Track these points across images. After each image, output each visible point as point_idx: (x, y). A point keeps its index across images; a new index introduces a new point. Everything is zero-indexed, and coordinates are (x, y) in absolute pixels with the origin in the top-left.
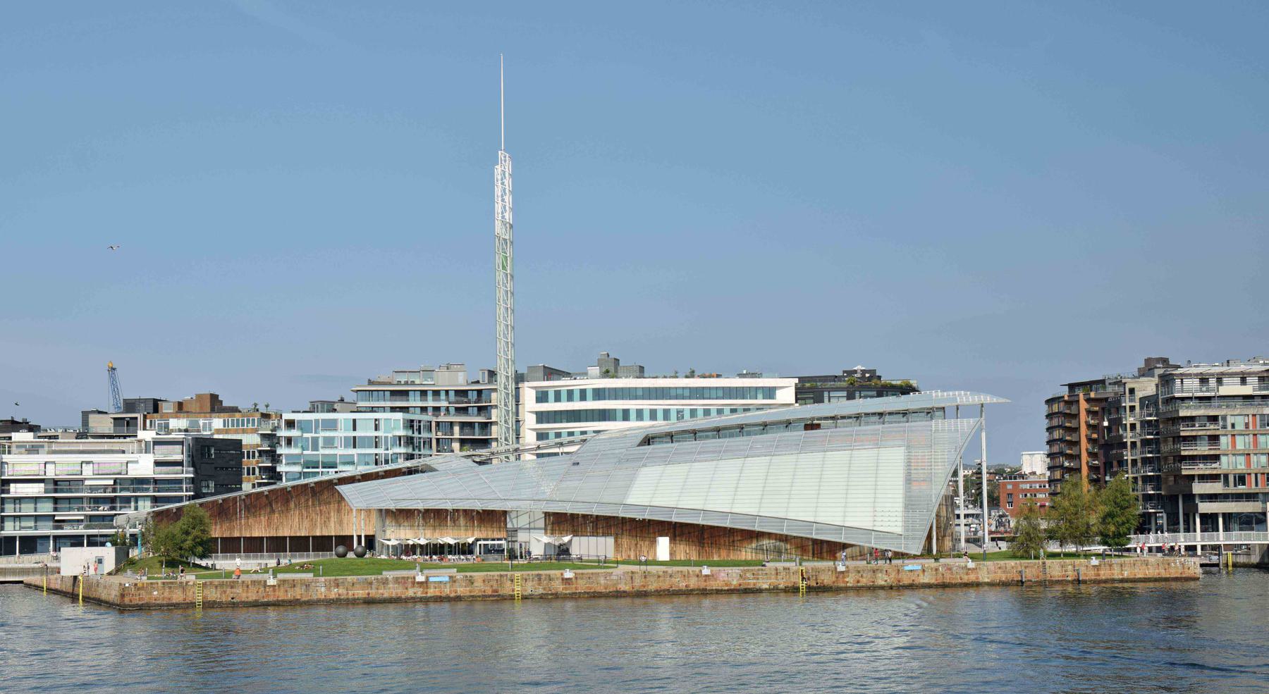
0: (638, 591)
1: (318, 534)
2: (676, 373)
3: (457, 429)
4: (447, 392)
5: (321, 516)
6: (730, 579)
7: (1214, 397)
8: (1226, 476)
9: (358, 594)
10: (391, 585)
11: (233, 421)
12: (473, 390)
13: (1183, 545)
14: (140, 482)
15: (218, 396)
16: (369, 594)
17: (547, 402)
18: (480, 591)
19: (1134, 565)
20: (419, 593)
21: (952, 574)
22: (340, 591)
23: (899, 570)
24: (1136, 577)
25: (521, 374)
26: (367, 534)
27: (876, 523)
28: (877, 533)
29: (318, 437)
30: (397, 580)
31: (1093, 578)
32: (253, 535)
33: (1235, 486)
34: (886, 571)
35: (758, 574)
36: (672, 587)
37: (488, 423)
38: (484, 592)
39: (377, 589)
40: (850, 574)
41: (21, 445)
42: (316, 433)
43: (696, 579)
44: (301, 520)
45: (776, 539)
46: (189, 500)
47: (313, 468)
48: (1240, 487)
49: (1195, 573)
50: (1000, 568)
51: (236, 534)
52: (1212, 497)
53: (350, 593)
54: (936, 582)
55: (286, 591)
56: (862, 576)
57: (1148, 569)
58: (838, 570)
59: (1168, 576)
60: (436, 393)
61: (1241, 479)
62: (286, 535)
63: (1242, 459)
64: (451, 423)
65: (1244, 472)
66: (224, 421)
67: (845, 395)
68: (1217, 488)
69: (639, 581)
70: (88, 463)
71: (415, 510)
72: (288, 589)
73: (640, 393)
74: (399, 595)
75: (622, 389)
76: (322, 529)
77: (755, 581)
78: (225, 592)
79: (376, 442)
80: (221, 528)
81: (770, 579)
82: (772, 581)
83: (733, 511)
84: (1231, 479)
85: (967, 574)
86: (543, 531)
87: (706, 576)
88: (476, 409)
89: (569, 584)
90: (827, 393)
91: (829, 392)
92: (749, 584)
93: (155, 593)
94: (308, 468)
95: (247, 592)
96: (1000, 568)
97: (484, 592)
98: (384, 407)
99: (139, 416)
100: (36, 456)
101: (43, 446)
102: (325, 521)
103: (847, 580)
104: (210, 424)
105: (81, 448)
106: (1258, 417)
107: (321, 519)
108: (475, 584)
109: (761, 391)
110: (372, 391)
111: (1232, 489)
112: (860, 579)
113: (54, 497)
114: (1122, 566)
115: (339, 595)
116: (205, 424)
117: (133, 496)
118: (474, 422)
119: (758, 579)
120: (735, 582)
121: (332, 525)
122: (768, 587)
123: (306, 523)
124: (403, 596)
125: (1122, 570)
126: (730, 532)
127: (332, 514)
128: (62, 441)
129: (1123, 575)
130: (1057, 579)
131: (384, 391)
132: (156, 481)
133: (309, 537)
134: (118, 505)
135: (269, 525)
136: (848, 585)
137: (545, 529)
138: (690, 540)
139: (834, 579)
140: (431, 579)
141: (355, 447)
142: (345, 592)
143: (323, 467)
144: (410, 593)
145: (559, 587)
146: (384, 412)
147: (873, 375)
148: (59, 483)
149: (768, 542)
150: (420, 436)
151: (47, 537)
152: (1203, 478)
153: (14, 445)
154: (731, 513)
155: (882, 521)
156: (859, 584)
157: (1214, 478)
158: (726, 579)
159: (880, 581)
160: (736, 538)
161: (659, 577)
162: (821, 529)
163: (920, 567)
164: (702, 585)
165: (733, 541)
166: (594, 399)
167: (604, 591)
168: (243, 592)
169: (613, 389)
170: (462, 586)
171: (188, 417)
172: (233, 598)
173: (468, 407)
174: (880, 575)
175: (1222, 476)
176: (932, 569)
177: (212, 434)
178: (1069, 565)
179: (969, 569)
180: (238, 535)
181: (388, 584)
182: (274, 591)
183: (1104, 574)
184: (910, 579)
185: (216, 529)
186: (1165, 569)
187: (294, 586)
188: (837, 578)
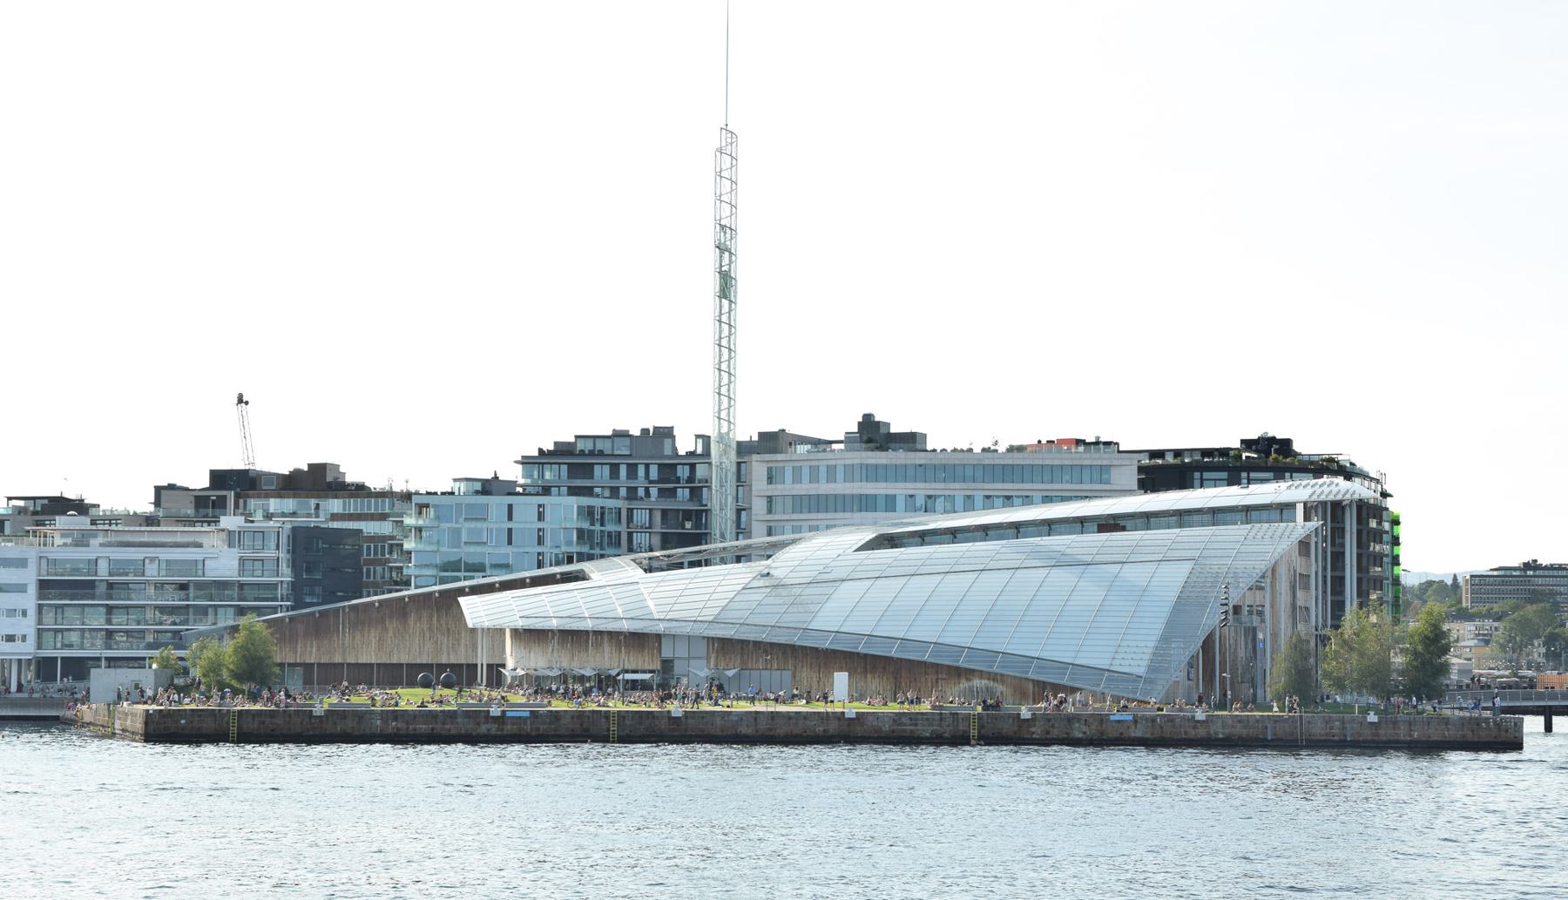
0: (763, 735)
5: (448, 636)
6: (880, 724)
9: (421, 729)
12: (684, 464)
14: (222, 585)
15: (339, 466)
16: (433, 729)
19: (1429, 723)
20: (494, 729)
21: (1174, 726)
22: (399, 725)
23: (1102, 720)
24: (1431, 739)
25: (1241, 443)
27: (1115, 662)
28: (1112, 674)
29: (461, 528)
31: (1369, 738)
32: (360, 662)
34: (1086, 720)
35: (917, 719)
36: (805, 732)
37: (703, 510)
38: (573, 730)
39: (443, 724)
40: (1037, 723)
42: (457, 522)
43: (837, 722)
44: (421, 641)
45: (989, 679)
46: (288, 611)
47: (453, 571)
49: (1515, 737)
50: (1240, 721)
51: (338, 659)
54: (1152, 737)
55: (335, 723)
56: (1053, 726)
57: (1448, 730)
59: (1477, 740)
62: (402, 662)
67: (1226, 477)
69: (764, 723)
70: (152, 560)
71: (549, 630)
74: (470, 732)
76: (449, 654)
77: (912, 728)
80: (319, 649)
81: (933, 726)
82: (935, 728)
83: (1076, 663)
86: (705, 661)
90: (1226, 477)
92: (905, 731)
93: (183, 722)
94: (447, 571)
96: (1240, 721)
99: (231, 495)
102: (453, 644)
103: (1033, 729)
105: (145, 539)
107: (448, 640)
108: (562, 721)
110: (543, 464)
112: (1051, 729)
114: (1410, 724)
115: (398, 729)
117: (211, 606)
121: (462, 648)
123: (429, 645)
124: (474, 733)
125: (1411, 730)
126: (937, 667)
127: (463, 635)
128: (165, 529)
129: (1411, 736)
130: (1318, 738)
131: (560, 464)
132: (241, 586)
135: (380, 647)
136: (1034, 736)
137: (708, 658)
138: (885, 678)
139: (1016, 728)
142: (405, 726)
143: (466, 571)
144: (483, 729)
148: (115, 586)
149: (978, 682)
150: (603, 528)
151: (99, 659)
154: (1072, 664)
155: (1126, 652)
156: (1048, 736)
158: (875, 723)
159: (1077, 732)
160: (940, 676)
162: (1044, 668)
163: (1131, 718)
165: (937, 680)
167: (720, 734)
170: (545, 723)
172: (272, 731)
173: (676, 488)
174: (1077, 725)
176: (1147, 719)
178: (1337, 721)
181: (456, 718)
183: (1385, 734)
185: (311, 652)
186: (1473, 731)
188: (1020, 727)
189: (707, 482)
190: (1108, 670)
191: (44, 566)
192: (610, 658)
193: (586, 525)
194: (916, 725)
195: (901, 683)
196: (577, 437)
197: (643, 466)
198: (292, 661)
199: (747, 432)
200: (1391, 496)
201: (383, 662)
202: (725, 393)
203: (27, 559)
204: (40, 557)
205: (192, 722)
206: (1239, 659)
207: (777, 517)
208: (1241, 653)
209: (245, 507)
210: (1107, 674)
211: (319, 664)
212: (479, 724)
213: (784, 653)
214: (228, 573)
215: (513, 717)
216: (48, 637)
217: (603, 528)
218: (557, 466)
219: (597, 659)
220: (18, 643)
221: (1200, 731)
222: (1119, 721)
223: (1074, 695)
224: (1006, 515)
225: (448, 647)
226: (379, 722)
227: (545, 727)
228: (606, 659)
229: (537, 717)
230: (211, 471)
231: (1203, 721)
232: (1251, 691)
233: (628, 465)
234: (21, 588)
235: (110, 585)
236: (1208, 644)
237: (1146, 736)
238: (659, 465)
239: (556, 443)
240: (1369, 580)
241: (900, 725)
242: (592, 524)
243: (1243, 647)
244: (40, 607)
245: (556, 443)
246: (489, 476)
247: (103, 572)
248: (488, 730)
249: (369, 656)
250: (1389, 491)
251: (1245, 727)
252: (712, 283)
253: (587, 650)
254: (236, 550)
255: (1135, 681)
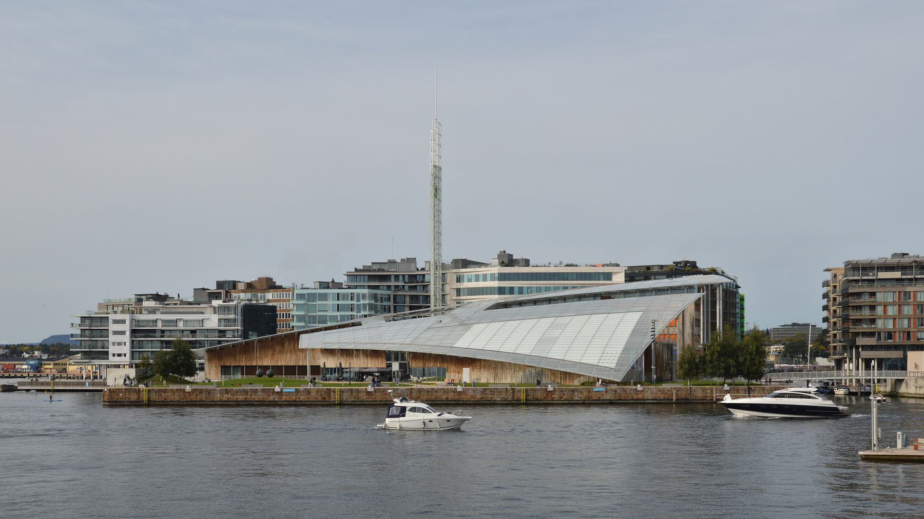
1: (301, 364)
2: (550, 264)
3: (408, 299)
4: (404, 276)
6: (476, 394)
7: (859, 280)
8: (879, 333)
10: (259, 394)
11: (277, 294)
12: (420, 275)
13: (876, 378)
16: (246, 398)
17: (479, 281)
18: (314, 398)
21: (626, 394)
22: (229, 396)
23: (589, 391)
26: (312, 365)
27: (601, 361)
28: (598, 367)
30: (263, 390)
33: (885, 340)
40: (556, 393)
41: (147, 309)
43: (453, 394)
48: (889, 341)
50: (660, 391)
51: (254, 364)
52: (872, 348)
53: (235, 397)
55: (197, 396)
56: (564, 394)
58: (548, 390)
60: (397, 277)
61: (890, 335)
62: (282, 365)
63: (891, 322)
64: (404, 295)
65: (891, 330)
66: (273, 294)
68: (872, 341)
72: (198, 395)
73: (602, 276)
75: (510, 273)
77: (492, 396)
78: (161, 395)
79: (352, 308)
80: (245, 360)
83: (581, 362)
84: (882, 335)
85: (637, 394)
87: (459, 392)
88: (422, 287)
89: (371, 395)
91: (655, 276)
93: (121, 395)
95: (174, 395)
96: (660, 391)
97: (317, 399)
98: (364, 286)
100: (154, 315)
101: (159, 310)
103: (554, 396)
104: (264, 296)
106: (902, 293)
109: (602, 275)
110: (357, 275)
111: (883, 342)
113: (161, 340)
116: (261, 296)
118: (420, 295)
119: (494, 395)
120: (478, 397)
122: (500, 399)
133: (296, 366)
134: (198, 345)
139: (545, 396)
140: (284, 390)
141: (338, 311)
144: (271, 398)
145: (363, 397)
146: (364, 288)
147: (693, 264)
150: (382, 304)
152: (865, 334)
153: (143, 309)
157: (872, 334)
161: (429, 392)
164: (457, 397)
166: (491, 281)
168: (171, 395)
169: (503, 273)
171: (251, 292)
172: (165, 399)
174: (576, 394)
175: (877, 333)
176: (612, 390)
177: (265, 303)
179: (638, 391)
180: (255, 365)
181: (258, 393)
182: (190, 395)
184: (597, 396)
187: (201, 392)
188: (547, 395)
189: (429, 282)
190: (597, 366)
191: (134, 323)
192: (364, 362)
193: (373, 302)
194: (494, 395)
195: (497, 373)
196: (373, 263)
197: (402, 276)
198: (234, 365)
199: (447, 259)
200: (740, 287)
201: (274, 365)
202: (437, 244)
203: (125, 320)
204: (132, 319)
205: (125, 395)
206: (664, 359)
207: (462, 298)
208: (665, 356)
209: (230, 297)
210: (596, 367)
211: (246, 366)
212: (269, 396)
213: (442, 359)
214: (214, 326)
215: (286, 392)
216: (136, 355)
217: (382, 304)
218: (363, 276)
219: (358, 363)
220: (123, 357)
221: (640, 395)
222: (598, 391)
223: (580, 378)
224: (558, 293)
225: (302, 358)
226: (219, 395)
227: (303, 397)
228: (362, 363)
229: (299, 392)
230: (217, 282)
231: (641, 391)
232: (670, 375)
233: (395, 275)
234: (123, 333)
235: (163, 331)
236: (648, 352)
237: (612, 399)
238: (409, 275)
239: (363, 266)
240: (730, 313)
241: (485, 394)
242: (376, 301)
243: (666, 353)
244: (133, 342)
245: (363, 266)
246: (330, 280)
247: (160, 326)
248: (274, 399)
249: (267, 362)
250: (739, 285)
251: (663, 393)
252: (430, 191)
253: (353, 359)
254: (216, 315)
255: (609, 371)
